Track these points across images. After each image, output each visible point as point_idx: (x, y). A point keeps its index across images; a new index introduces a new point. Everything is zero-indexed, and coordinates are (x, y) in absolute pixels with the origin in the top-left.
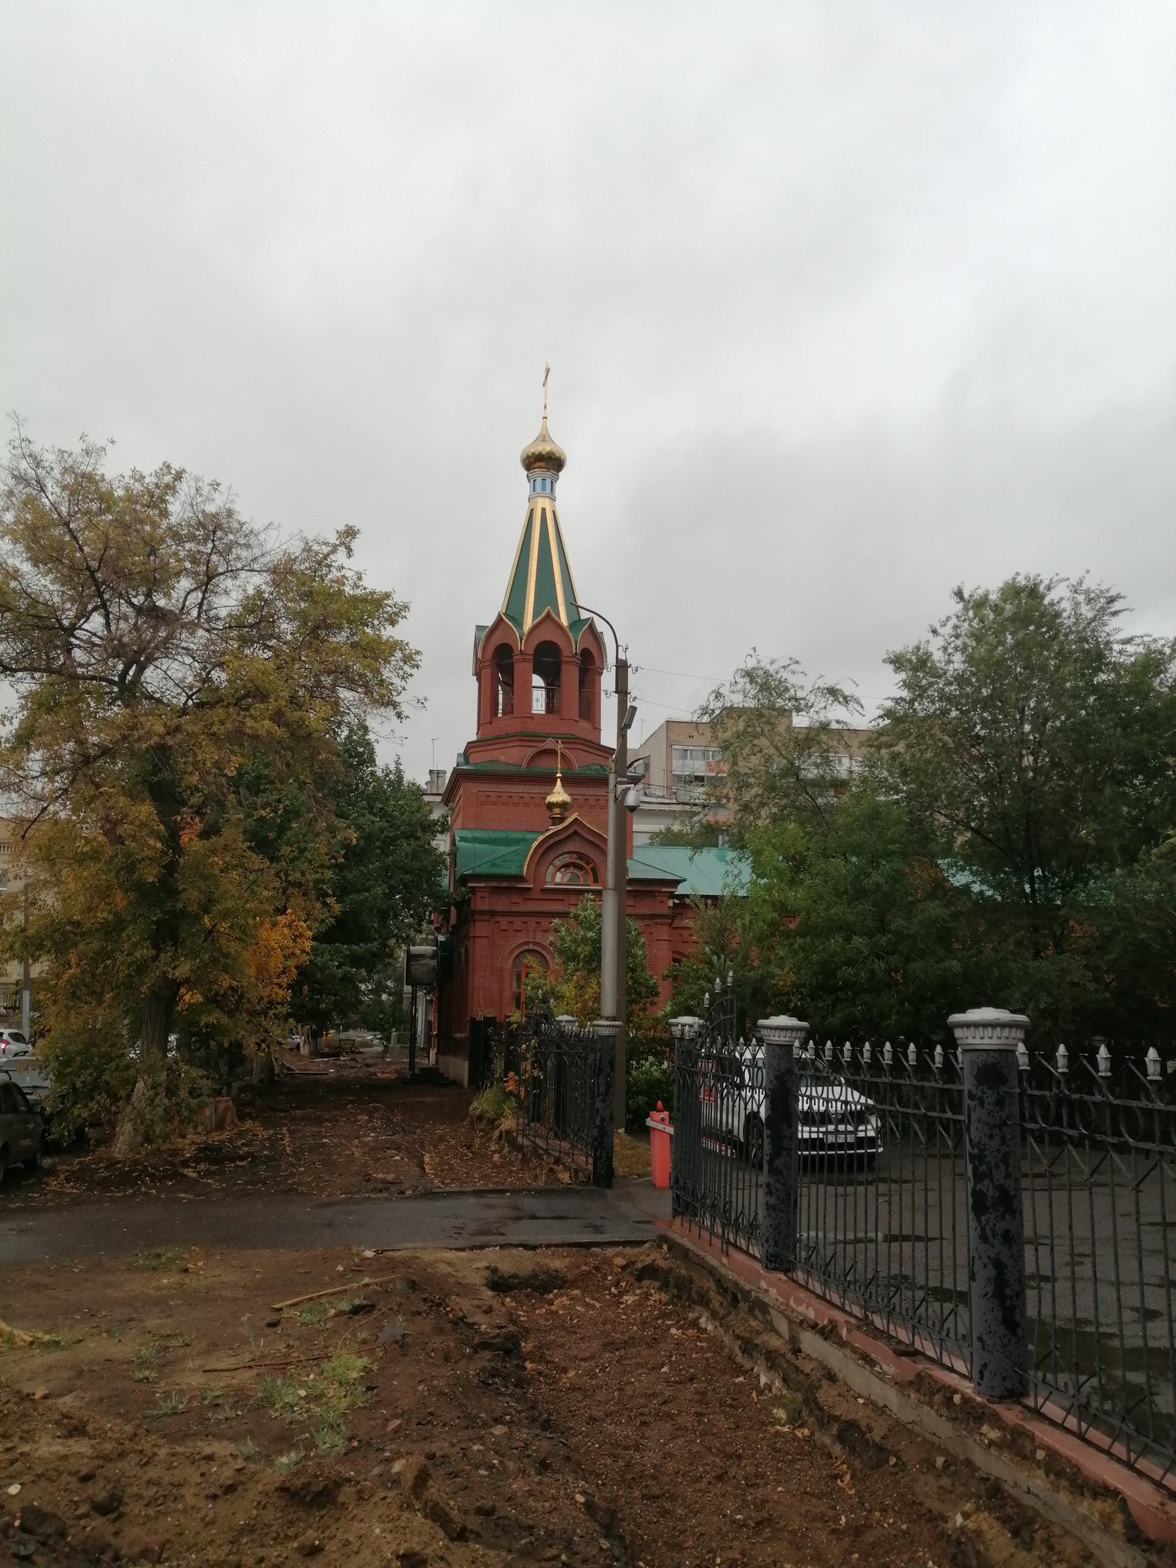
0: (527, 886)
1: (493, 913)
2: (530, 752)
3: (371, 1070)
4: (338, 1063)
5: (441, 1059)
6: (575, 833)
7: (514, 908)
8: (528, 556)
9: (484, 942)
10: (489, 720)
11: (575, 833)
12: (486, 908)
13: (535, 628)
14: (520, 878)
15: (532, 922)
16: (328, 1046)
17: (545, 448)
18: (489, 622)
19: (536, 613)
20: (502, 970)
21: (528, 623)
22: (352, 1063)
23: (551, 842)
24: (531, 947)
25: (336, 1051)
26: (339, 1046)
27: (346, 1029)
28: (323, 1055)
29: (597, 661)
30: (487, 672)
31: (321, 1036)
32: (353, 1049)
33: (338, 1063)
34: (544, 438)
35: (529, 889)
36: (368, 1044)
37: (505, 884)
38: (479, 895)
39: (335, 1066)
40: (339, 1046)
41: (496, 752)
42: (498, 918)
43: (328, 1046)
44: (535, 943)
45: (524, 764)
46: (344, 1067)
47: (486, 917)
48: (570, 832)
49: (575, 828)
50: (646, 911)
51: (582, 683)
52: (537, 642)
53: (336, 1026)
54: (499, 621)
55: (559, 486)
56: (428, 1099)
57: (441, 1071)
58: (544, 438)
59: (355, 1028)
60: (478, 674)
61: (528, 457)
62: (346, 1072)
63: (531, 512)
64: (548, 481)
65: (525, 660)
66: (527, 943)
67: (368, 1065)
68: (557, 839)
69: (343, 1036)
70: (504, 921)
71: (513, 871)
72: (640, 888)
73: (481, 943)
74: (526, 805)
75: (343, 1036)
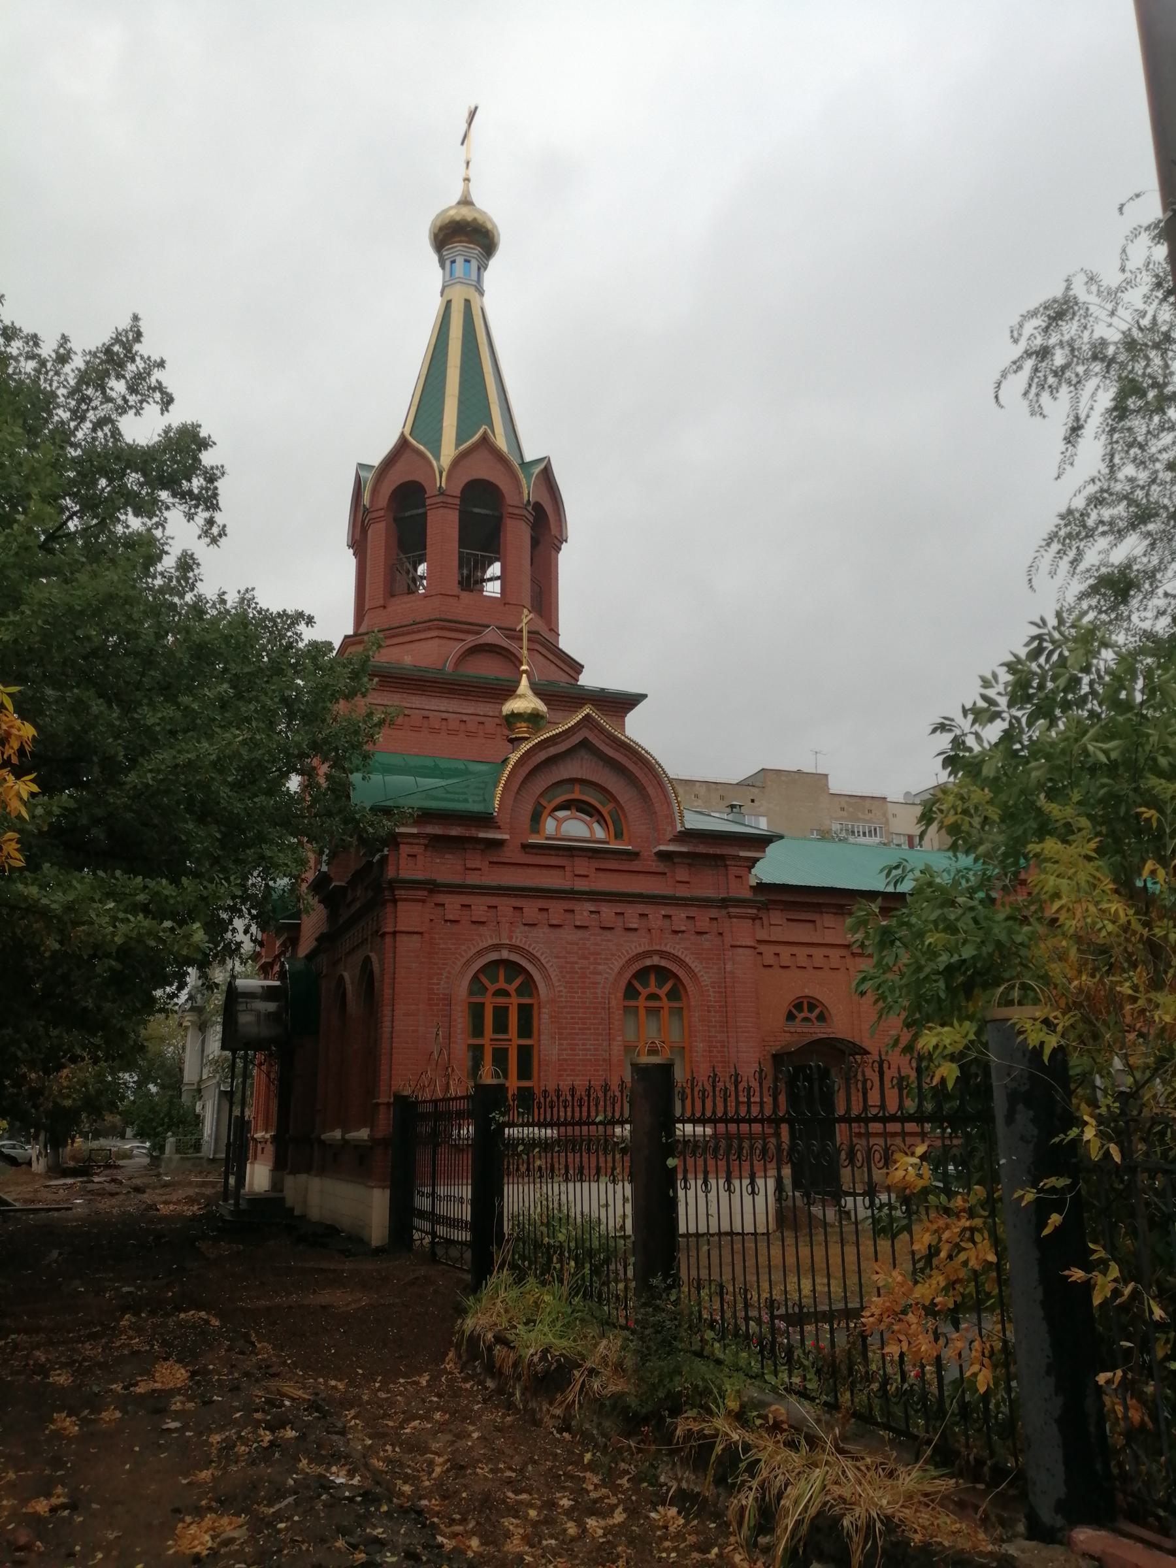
0: (498, 836)
1: (433, 887)
2: (457, 648)
3: (147, 1197)
4: (90, 1186)
5: (290, 1181)
6: (585, 744)
7: (473, 879)
8: (446, 355)
9: (414, 942)
10: (381, 602)
11: (585, 744)
12: (419, 876)
13: (456, 462)
14: (486, 820)
15: (505, 905)
16: (73, 1158)
17: (466, 213)
18: (375, 458)
19: (459, 441)
20: (448, 1000)
21: (449, 450)
22: (112, 1187)
23: (542, 756)
24: (505, 954)
25: (84, 1169)
26: (90, 1159)
27: (96, 1136)
28: (66, 1173)
29: (553, 527)
30: (378, 532)
31: (65, 1145)
32: (109, 1163)
33: (90, 1186)
34: (466, 201)
35: (500, 843)
36: (128, 1155)
37: (455, 831)
38: (405, 850)
39: (85, 1192)
40: (90, 1159)
41: (395, 650)
42: (441, 898)
43: (73, 1158)
44: (513, 948)
45: (449, 666)
46: (102, 1193)
47: (421, 894)
48: (575, 739)
49: (585, 733)
50: (710, 893)
51: (535, 543)
52: (465, 480)
53: (85, 1136)
54: (403, 445)
55: (488, 276)
56: (340, 1299)
57: (289, 1203)
58: (466, 201)
59: (106, 1136)
60: (358, 543)
61: (441, 229)
62: (104, 1205)
63: (448, 304)
64: (474, 264)
65: (445, 505)
66: (497, 947)
67: (138, 1190)
68: (553, 751)
69: (95, 1144)
70: (453, 903)
71: (473, 806)
72: (702, 849)
73: (407, 945)
74: (452, 733)
75: (95, 1144)
